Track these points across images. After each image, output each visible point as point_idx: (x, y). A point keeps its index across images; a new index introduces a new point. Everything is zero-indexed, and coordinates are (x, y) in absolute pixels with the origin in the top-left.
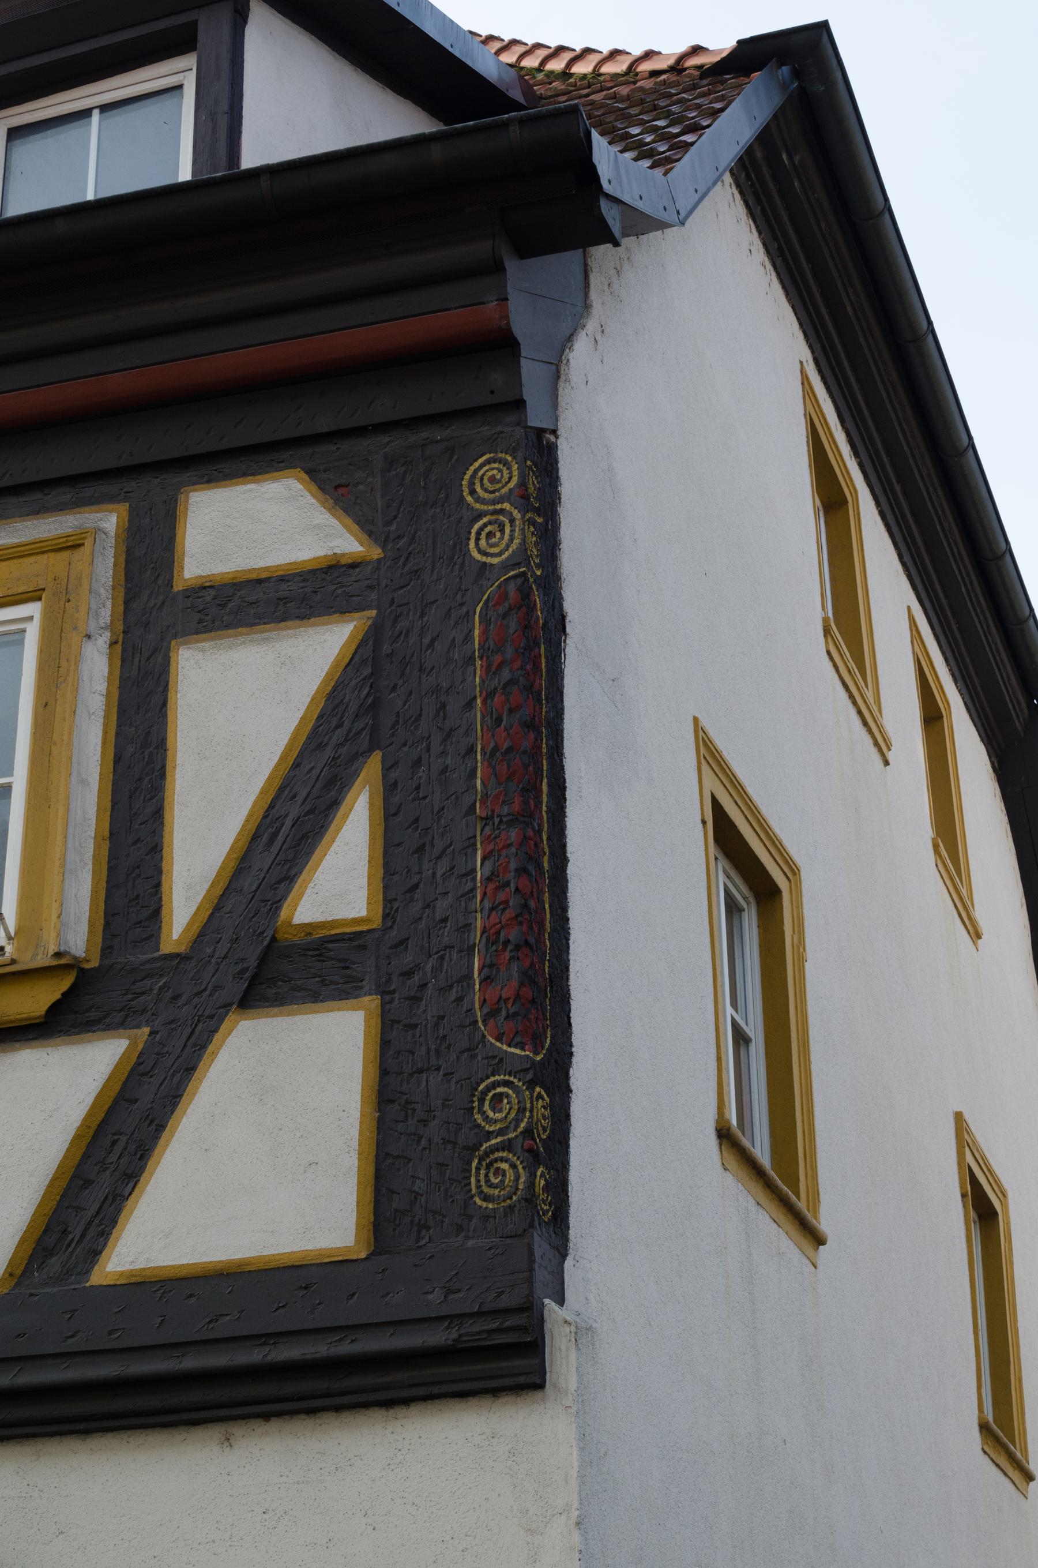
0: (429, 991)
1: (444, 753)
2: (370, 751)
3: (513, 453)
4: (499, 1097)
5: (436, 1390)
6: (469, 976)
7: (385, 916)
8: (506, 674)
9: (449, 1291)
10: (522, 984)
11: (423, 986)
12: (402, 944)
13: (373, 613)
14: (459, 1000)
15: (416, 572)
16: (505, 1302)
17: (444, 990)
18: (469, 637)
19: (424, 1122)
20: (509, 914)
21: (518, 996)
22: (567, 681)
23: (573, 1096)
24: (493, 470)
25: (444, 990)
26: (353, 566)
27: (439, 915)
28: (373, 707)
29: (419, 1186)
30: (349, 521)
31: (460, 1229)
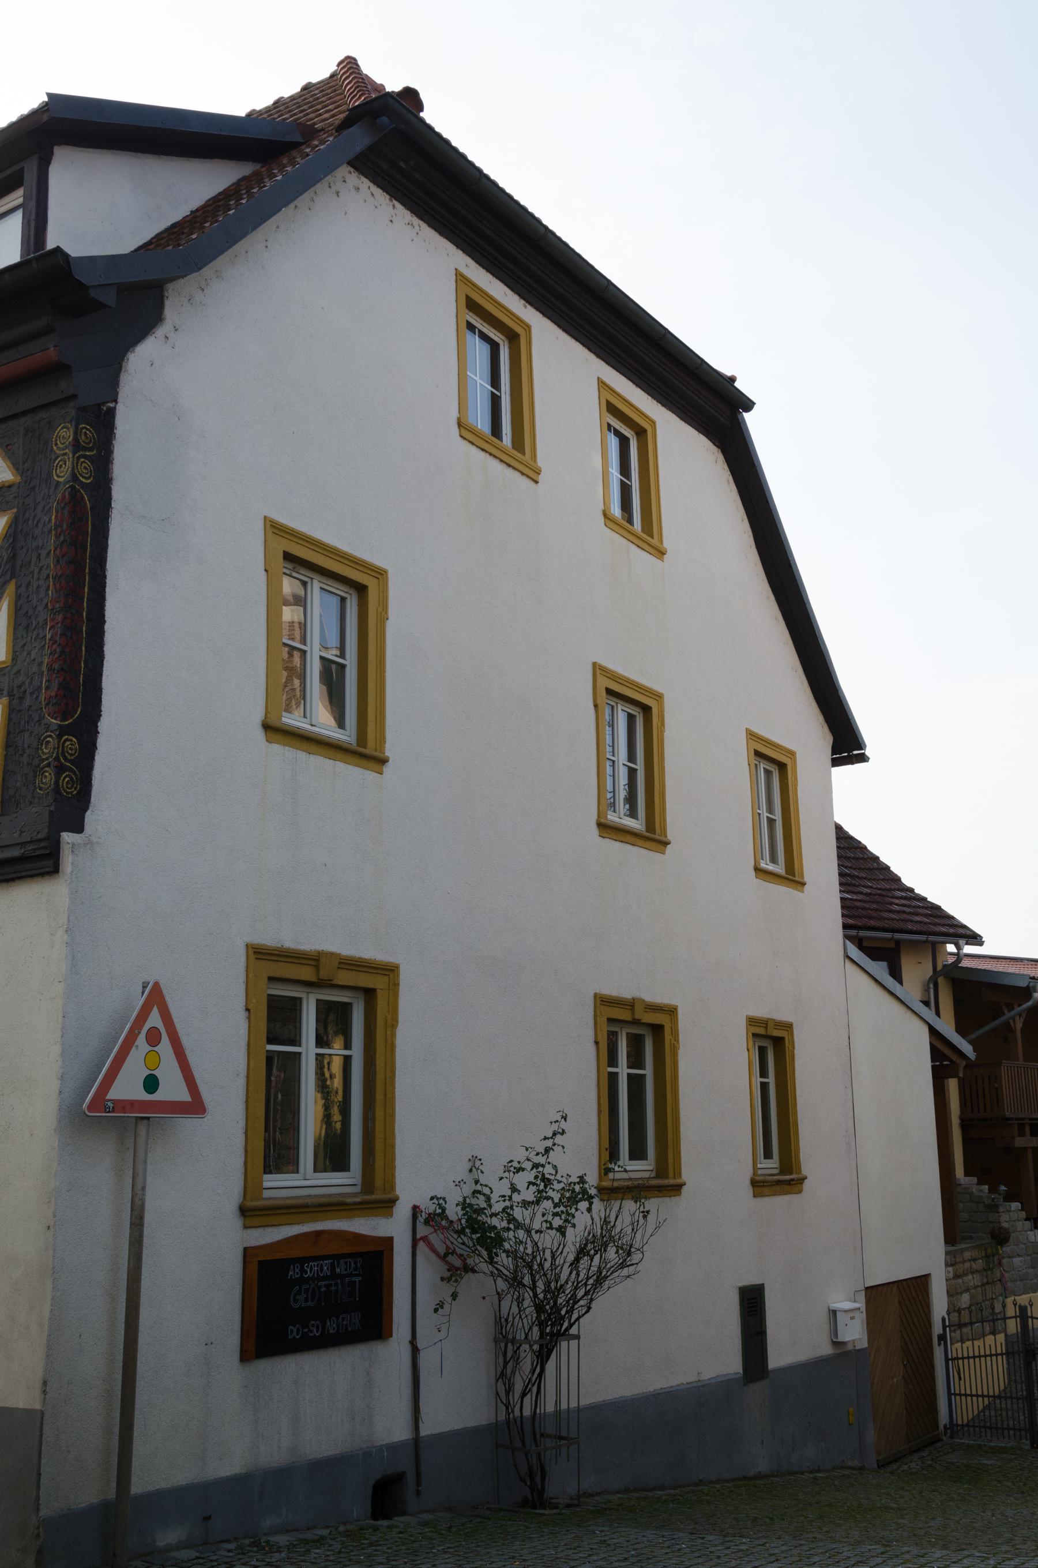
0: (27, 693)
1: (38, 579)
2: (11, 579)
3: (70, 422)
4: (48, 742)
5: (19, 875)
6: (41, 687)
7: (13, 660)
8: (62, 538)
9: (22, 832)
10: (59, 689)
11: (25, 692)
12: (18, 672)
13: (15, 510)
14: (37, 697)
15: (33, 488)
16: (40, 836)
17: (32, 694)
18: (50, 521)
19: (22, 755)
20: (56, 656)
21: (56, 695)
22: (111, 542)
23: (99, 735)
24: (63, 433)
25: (32, 694)
26: (10, 486)
27: (33, 657)
28: (13, 557)
29: (18, 785)
30: (9, 464)
31: (31, 803)
